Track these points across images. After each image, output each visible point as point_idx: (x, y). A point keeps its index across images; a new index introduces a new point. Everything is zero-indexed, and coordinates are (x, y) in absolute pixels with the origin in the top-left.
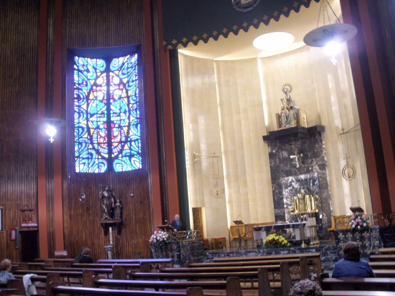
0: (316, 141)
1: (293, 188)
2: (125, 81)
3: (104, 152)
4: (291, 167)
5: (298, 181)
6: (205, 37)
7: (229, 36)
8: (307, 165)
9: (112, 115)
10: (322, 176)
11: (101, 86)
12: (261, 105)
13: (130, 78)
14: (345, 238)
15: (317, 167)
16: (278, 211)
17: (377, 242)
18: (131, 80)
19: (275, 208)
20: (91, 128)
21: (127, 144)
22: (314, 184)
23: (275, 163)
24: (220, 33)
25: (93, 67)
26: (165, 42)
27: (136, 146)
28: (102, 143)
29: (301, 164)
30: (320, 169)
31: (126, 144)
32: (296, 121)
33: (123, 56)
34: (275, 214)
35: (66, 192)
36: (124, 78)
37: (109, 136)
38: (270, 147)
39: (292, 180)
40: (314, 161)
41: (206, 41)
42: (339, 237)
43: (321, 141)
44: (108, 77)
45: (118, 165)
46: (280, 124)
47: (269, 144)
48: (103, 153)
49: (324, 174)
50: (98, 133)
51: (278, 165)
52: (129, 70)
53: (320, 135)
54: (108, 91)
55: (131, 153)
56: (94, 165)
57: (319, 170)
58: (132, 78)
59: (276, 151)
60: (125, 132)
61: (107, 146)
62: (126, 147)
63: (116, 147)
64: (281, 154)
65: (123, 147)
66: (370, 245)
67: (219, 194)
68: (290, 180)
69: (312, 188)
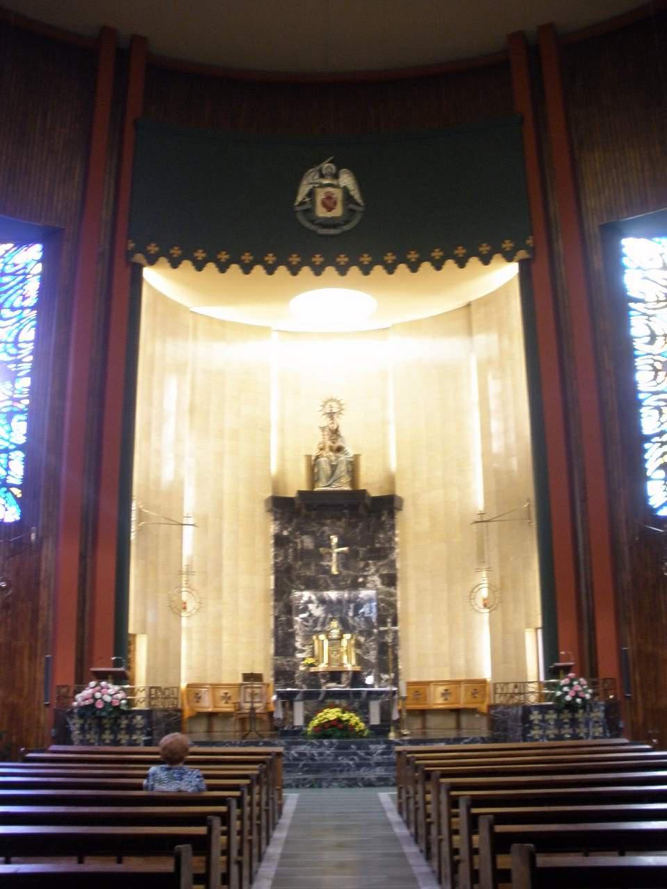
0: (381, 526)
1: (311, 615)
4: (318, 572)
5: (322, 601)
7: (276, 272)
10: (388, 599)
12: (266, 429)
13: (6, 300)
14: (543, 721)
15: (376, 578)
16: (282, 661)
19: (277, 653)
22: (356, 614)
23: (286, 557)
24: (259, 260)
26: (132, 243)
29: (341, 569)
30: (383, 583)
35: (626, 578)
39: (310, 597)
41: (223, 268)
42: (532, 717)
43: (393, 527)
46: (313, 476)
47: (278, 515)
49: (392, 595)
51: (292, 563)
53: (392, 515)
57: (380, 586)
58: (12, 299)
59: (290, 532)
66: (587, 735)
69: (351, 621)
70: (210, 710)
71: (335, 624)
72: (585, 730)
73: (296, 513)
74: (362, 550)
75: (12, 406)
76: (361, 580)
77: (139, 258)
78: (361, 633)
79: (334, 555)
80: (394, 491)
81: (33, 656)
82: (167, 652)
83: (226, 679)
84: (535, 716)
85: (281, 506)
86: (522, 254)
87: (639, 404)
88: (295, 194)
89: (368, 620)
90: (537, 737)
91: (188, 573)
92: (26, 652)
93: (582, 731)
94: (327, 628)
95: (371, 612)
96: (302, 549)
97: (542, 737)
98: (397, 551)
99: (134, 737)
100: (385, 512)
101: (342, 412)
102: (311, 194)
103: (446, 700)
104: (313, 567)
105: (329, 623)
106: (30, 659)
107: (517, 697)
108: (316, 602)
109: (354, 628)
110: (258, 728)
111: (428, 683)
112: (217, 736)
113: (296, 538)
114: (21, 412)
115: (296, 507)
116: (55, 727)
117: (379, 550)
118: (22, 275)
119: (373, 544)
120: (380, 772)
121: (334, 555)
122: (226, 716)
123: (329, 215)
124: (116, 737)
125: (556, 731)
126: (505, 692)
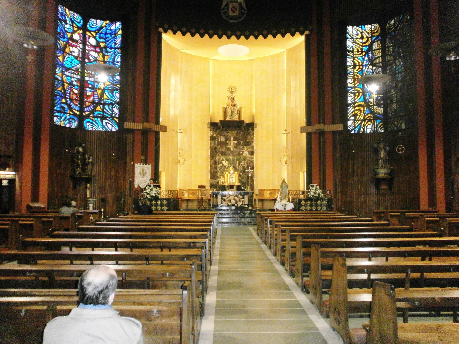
0: (249, 134)
1: (223, 165)
2: (102, 45)
3: (76, 108)
4: (226, 149)
6: (184, 31)
8: (239, 149)
9: (86, 75)
11: (76, 41)
14: (306, 204)
16: (213, 181)
17: (325, 208)
18: (109, 46)
19: (211, 178)
20: (65, 83)
21: (100, 106)
22: (239, 164)
23: (215, 144)
25: (71, 19)
27: (110, 110)
28: (74, 100)
29: (235, 149)
31: (99, 106)
32: (238, 116)
33: (101, 19)
34: (210, 183)
36: (101, 42)
37: (82, 93)
38: (212, 132)
39: (223, 159)
40: (245, 148)
42: (302, 203)
44: (84, 35)
45: (88, 124)
47: (212, 129)
48: (74, 109)
50: (71, 89)
52: (107, 36)
54: (84, 49)
55: (103, 115)
56: (66, 120)
58: (110, 44)
59: (216, 135)
60: (98, 93)
61: (79, 103)
62: (98, 108)
63: (88, 106)
64: (219, 138)
65: (95, 108)
66: (321, 209)
67: (180, 163)
68: (221, 159)
69: (237, 167)
70: (187, 198)
71: (231, 168)
72: (320, 208)
73: (219, 128)
74: (242, 142)
75: (113, 87)
76: (241, 153)
77: (161, 30)
78: (241, 172)
79: (232, 144)
80: (254, 121)
81: (125, 180)
82: (173, 178)
83: (193, 188)
84: (303, 202)
85: (213, 126)
86: (307, 32)
87: (347, 92)
88: (221, 4)
89: (243, 167)
90: (303, 210)
91: (180, 150)
92: (122, 178)
93: (319, 208)
94: (229, 170)
95: (245, 164)
96: (220, 141)
97: (305, 210)
98: (254, 143)
99: (163, 208)
100: (251, 129)
101: (236, 91)
102: (227, 5)
103: (270, 196)
104: (224, 148)
105: (230, 168)
106: (124, 180)
107: (297, 196)
108: (225, 160)
109: (238, 170)
110: (204, 205)
111: (264, 190)
112: (190, 207)
113: (218, 137)
114: (117, 90)
115: (219, 126)
116: (134, 204)
117: (248, 142)
118: (114, 33)
119: (246, 140)
120: (248, 220)
121: (232, 144)
122: (192, 200)
123: (234, 14)
124: (156, 208)
125: (310, 208)
126: (292, 193)
